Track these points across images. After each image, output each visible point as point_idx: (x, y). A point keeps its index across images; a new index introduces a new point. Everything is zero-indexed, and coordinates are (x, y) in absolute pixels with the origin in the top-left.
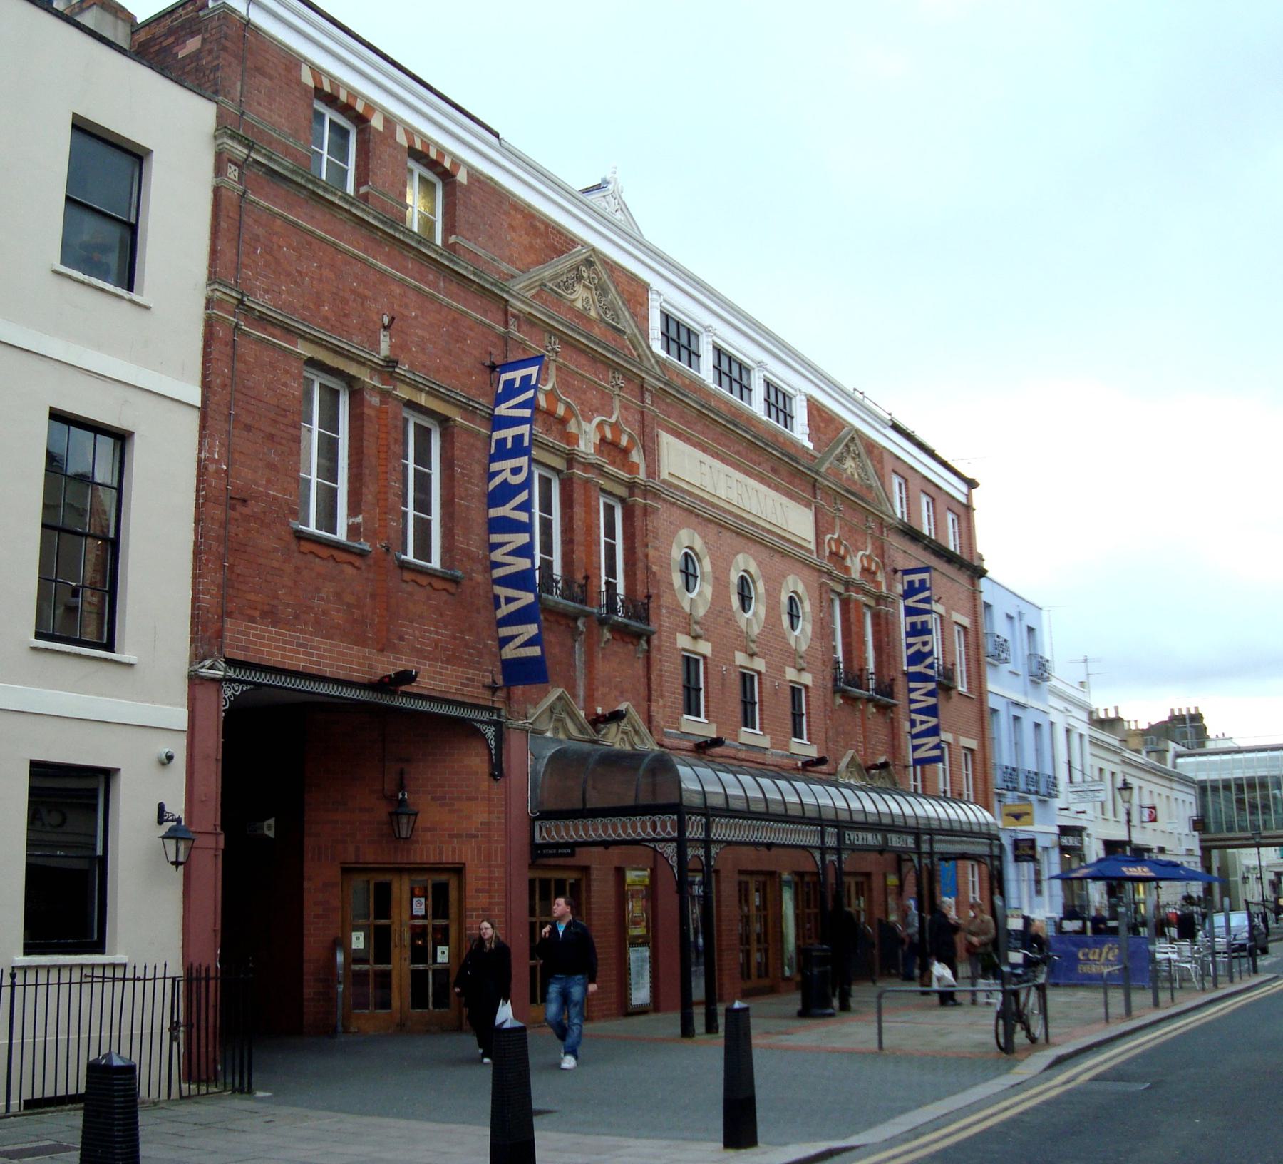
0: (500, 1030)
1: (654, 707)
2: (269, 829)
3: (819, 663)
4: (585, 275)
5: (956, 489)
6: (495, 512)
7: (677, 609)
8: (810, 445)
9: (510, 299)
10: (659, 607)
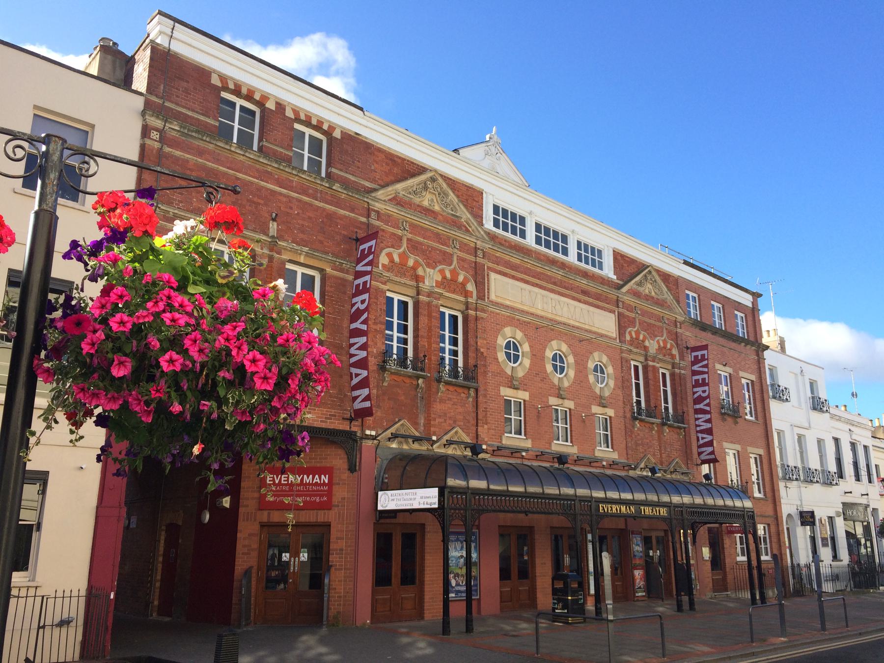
1: (480, 429)
3: (621, 403)
4: (430, 186)
5: (746, 300)
7: (502, 372)
8: (615, 277)
9: (370, 202)
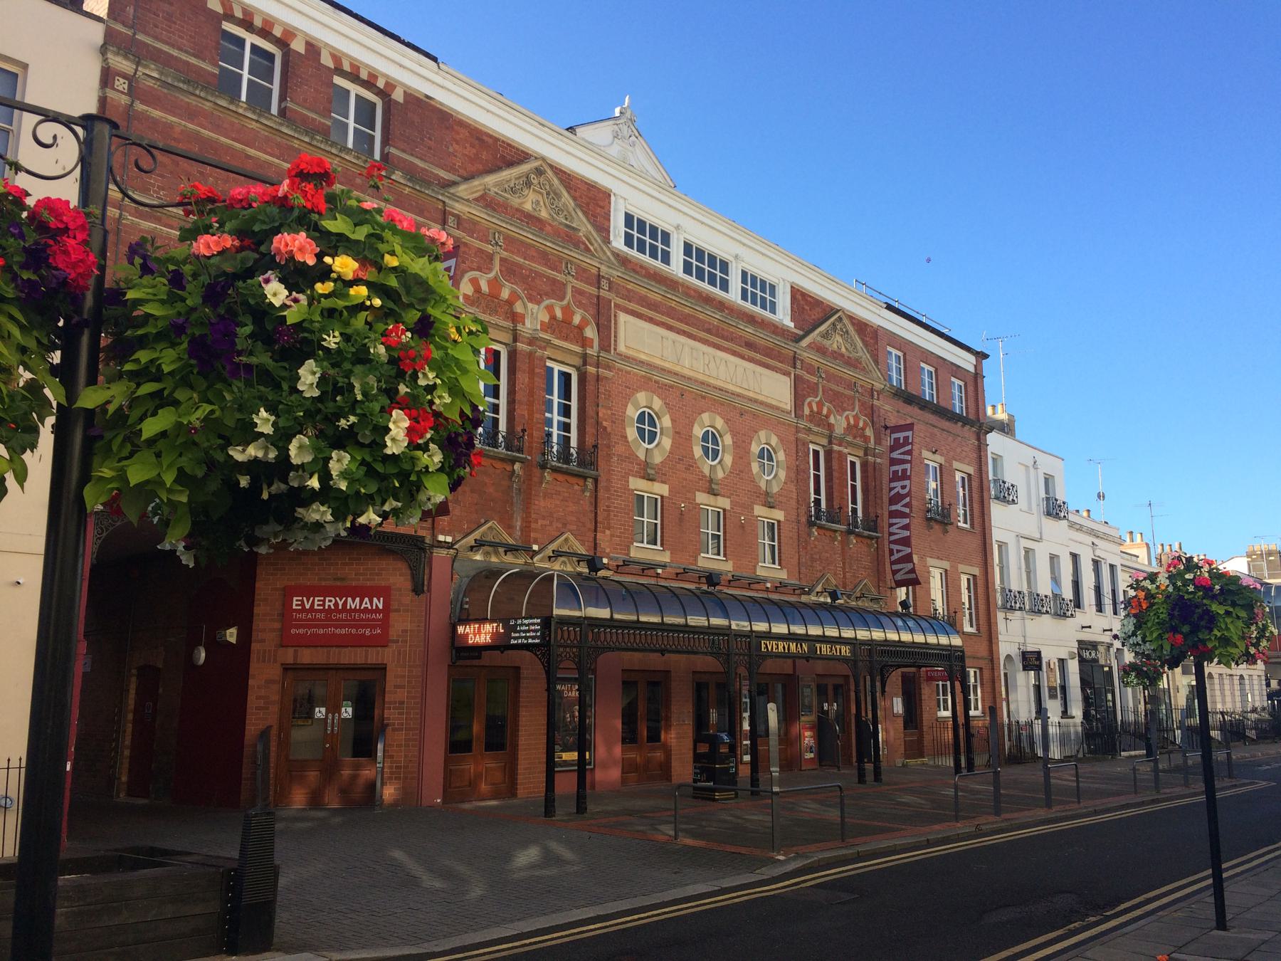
0: (395, 804)
2: (231, 635)
3: (794, 503)
4: (535, 182)
5: (966, 361)
6: (894, 508)
7: (632, 457)
9: (447, 200)
10: (609, 456)
